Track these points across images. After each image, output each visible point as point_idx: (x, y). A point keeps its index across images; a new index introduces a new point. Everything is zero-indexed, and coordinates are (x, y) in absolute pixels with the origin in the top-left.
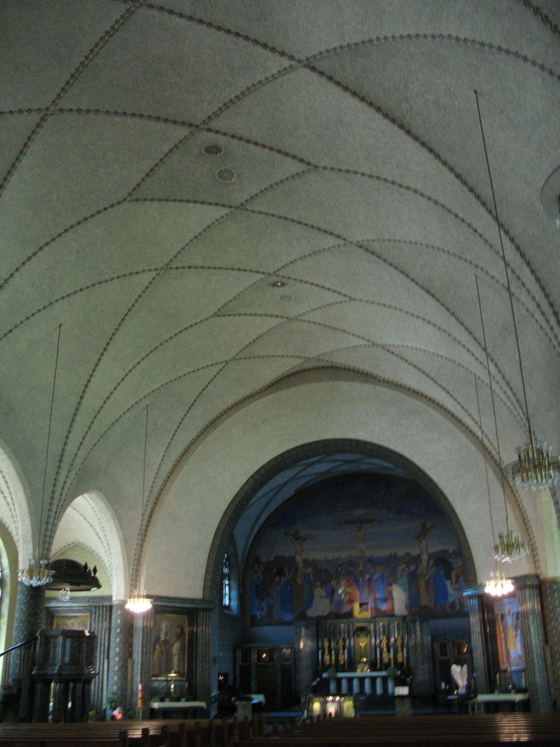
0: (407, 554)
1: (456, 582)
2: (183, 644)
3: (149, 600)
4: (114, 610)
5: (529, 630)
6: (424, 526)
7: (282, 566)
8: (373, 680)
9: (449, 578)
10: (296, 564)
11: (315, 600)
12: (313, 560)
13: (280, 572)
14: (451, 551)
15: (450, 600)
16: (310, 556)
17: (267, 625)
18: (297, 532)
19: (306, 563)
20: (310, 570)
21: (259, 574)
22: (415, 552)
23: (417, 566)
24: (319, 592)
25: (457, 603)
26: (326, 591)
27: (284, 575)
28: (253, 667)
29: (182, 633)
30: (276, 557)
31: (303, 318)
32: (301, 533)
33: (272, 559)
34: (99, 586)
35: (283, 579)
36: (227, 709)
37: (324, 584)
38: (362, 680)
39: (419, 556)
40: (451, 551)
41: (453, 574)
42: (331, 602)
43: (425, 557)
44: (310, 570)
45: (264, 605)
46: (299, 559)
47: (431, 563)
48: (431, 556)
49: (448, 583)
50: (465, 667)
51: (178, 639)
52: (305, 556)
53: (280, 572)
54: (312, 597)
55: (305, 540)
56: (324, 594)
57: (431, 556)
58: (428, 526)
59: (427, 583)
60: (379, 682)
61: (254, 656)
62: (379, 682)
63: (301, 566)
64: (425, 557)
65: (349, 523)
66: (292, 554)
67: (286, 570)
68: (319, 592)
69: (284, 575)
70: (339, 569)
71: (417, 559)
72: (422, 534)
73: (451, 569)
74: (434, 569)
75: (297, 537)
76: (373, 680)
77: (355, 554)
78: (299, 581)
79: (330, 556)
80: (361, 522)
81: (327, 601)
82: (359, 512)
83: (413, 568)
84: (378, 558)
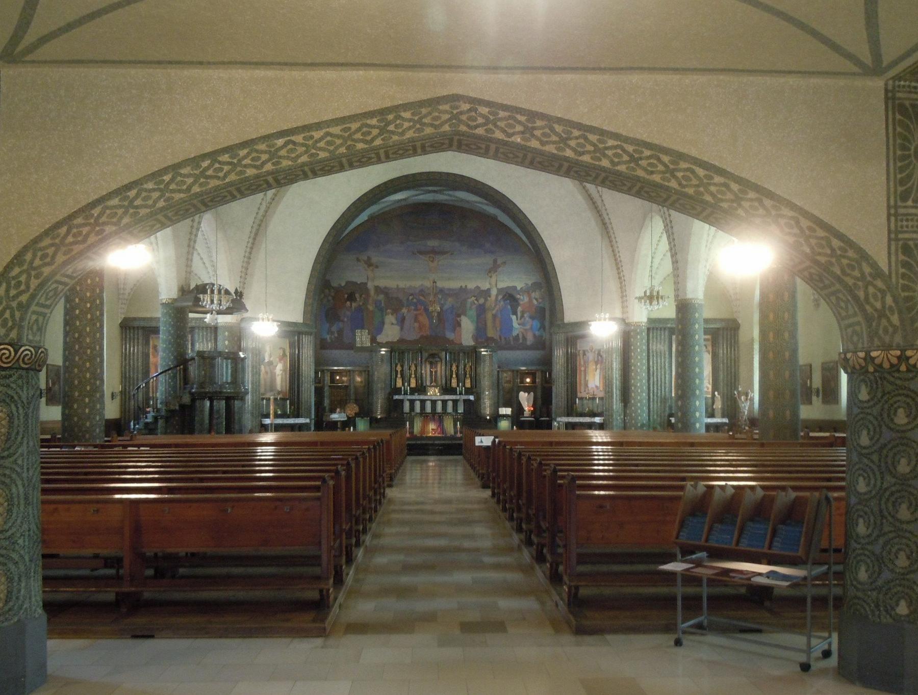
0: (478, 287)
1: (522, 316)
2: (285, 366)
3: (275, 323)
4: (219, 332)
5: (612, 364)
6: (495, 261)
7: (353, 292)
8: (445, 402)
9: (515, 313)
10: (367, 290)
11: (386, 326)
12: (385, 288)
13: (351, 298)
14: (519, 288)
15: (515, 333)
16: (382, 283)
17: (337, 348)
18: (369, 258)
19: (378, 289)
20: (381, 297)
21: (330, 298)
22: (485, 286)
23: (486, 300)
24: (390, 319)
25: (521, 336)
26: (397, 319)
27: (355, 300)
28: (326, 388)
29: (284, 355)
30: (347, 283)
31: (856, 69)
32: (374, 260)
33: (343, 284)
34: (247, 311)
35: (354, 305)
36: (321, 424)
37: (395, 311)
38: (434, 402)
39: (489, 290)
40: (519, 288)
41: (520, 309)
42: (402, 329)
43: (494, 292)
44: (381, 297)
45: (334, 328)
46: (370, 285)
47: (500, 297)
48: (500, 291)
49: (514, 317)
50: (532, 394)
51: (280, 360)
52: (377, 283)
53: (351, 298)
54: (383, 323)
55: (377, 267)
56: (394, 321)
57: (500, 291)
58: (499, 262)
59: (494, 316)
60: (450, 404)
61: (327, 378)
62: (450, 404)
63: (372, 292)
64: (494, 292)
65: (421, 253)
66: (364, 281)
67: (357, 296)
68: (390, 319)
69: (355, 300)
70: (411, 298)
71: (487, 293)
72: (493, 269)
73: (518, 305)
74: (502, 303)
75: (369, 263)
76: (445, 402)
77: (428, 284)
78: (371, 308)
79: (402, 284)
80: (435, 253)
81: (397, 328)
82: (432, 243)
83: (482, 301)
84: (449, 289)
